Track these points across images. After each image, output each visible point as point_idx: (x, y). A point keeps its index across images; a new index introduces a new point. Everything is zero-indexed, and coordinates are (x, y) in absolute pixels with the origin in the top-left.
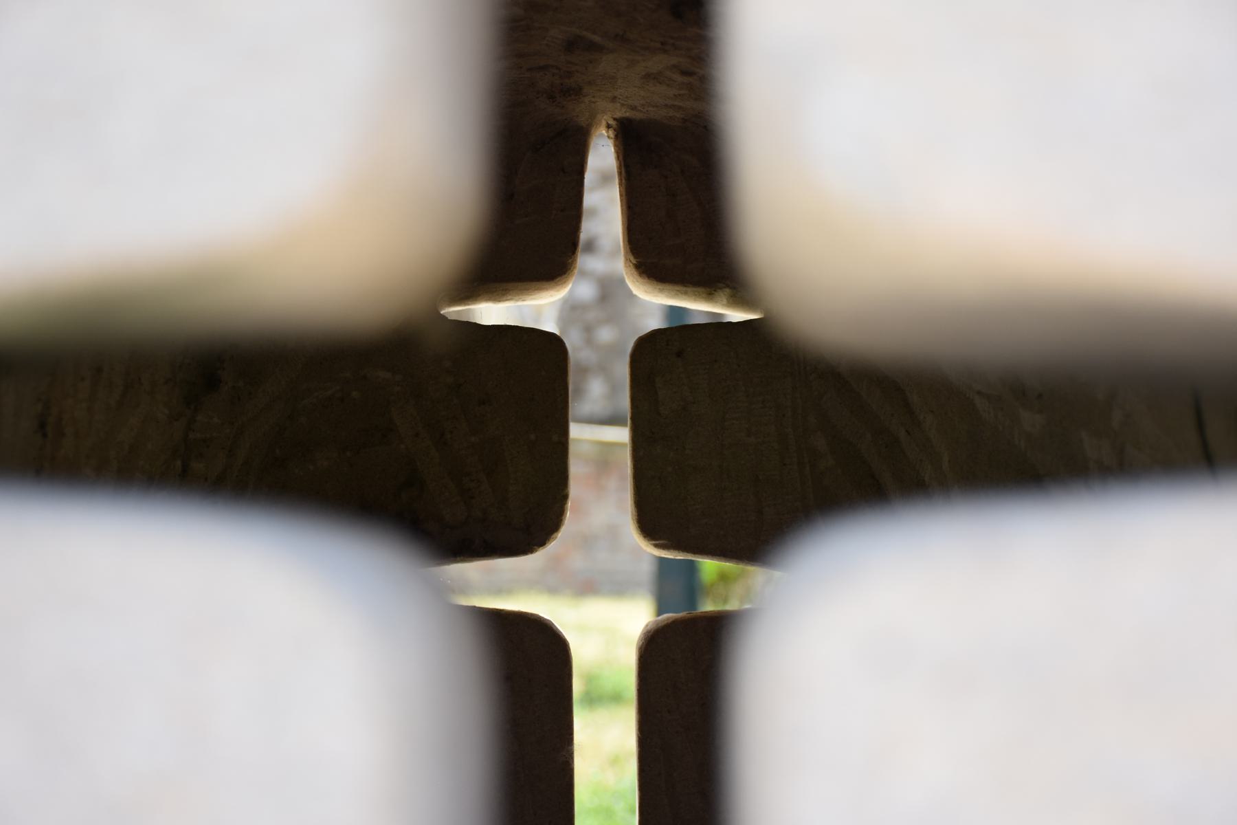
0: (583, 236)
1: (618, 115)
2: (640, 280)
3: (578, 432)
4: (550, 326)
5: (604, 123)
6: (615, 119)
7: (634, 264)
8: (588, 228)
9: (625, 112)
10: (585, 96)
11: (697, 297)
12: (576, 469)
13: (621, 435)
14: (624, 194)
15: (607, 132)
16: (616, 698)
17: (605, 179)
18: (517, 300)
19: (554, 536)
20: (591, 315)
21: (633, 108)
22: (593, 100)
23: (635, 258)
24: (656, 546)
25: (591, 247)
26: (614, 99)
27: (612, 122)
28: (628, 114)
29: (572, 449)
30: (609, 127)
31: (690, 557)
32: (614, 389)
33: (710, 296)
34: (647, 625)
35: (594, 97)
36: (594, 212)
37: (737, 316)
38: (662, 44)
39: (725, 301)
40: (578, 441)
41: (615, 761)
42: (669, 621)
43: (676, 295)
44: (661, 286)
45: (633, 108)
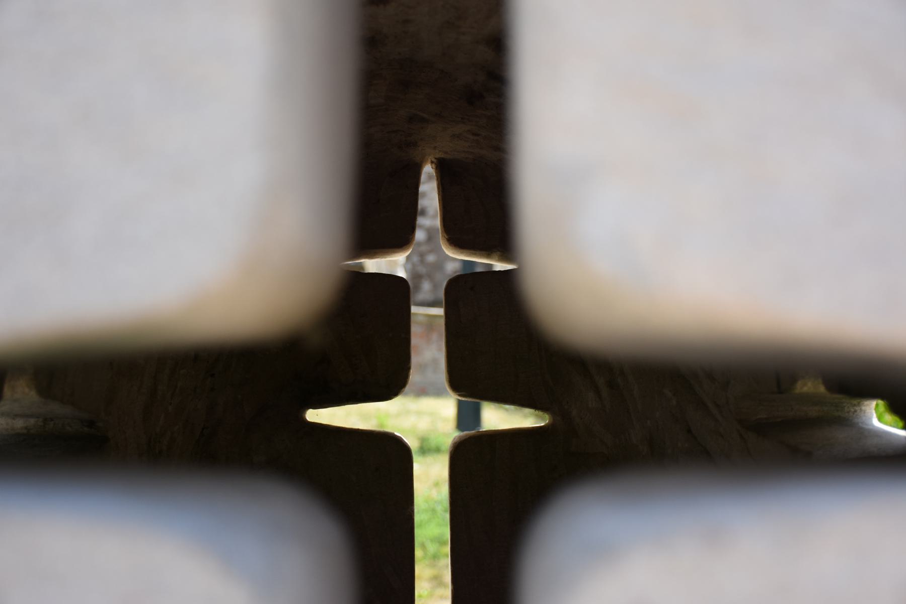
0: (419, 207)
1: (438, 156)
2: (450, 247)
3: (414, 309)
4: (402, 274)
5: (429, 160)
6: (436, 158)
7: (446, 239)
8: (422, 203)
9: (441, 155)
10: (419, 146)
11: (482, 256)
12: (415, 330)
13: (440, 311)
14: (441, 199)
15: (431, 165)
16: (446, 598)
17: (430, 178)
18: (382, 258)
19: (402, 390)
20: (424, 248)
21: (446, 153)
22: (423, 148)
23: (447, 235)
24: (459, 395)
25: (423, 213)
26: (435, 148)
27: (433, 160)
28: (442, 156)
29: (413, 318)
30: (432, 162)
31: (478, 401)
32: (435, 287)
33: (488, 256)
34: (454, 439)
35: (424, 147)
36: (424, 194)
37: (500, 266)
38: (462, 118)
39: (497, 259)
40: (416, 314)
41: (437, 484)
42: (467, 437)
43: (469, 255)
44: (462, 251)
45: (446, 153)
